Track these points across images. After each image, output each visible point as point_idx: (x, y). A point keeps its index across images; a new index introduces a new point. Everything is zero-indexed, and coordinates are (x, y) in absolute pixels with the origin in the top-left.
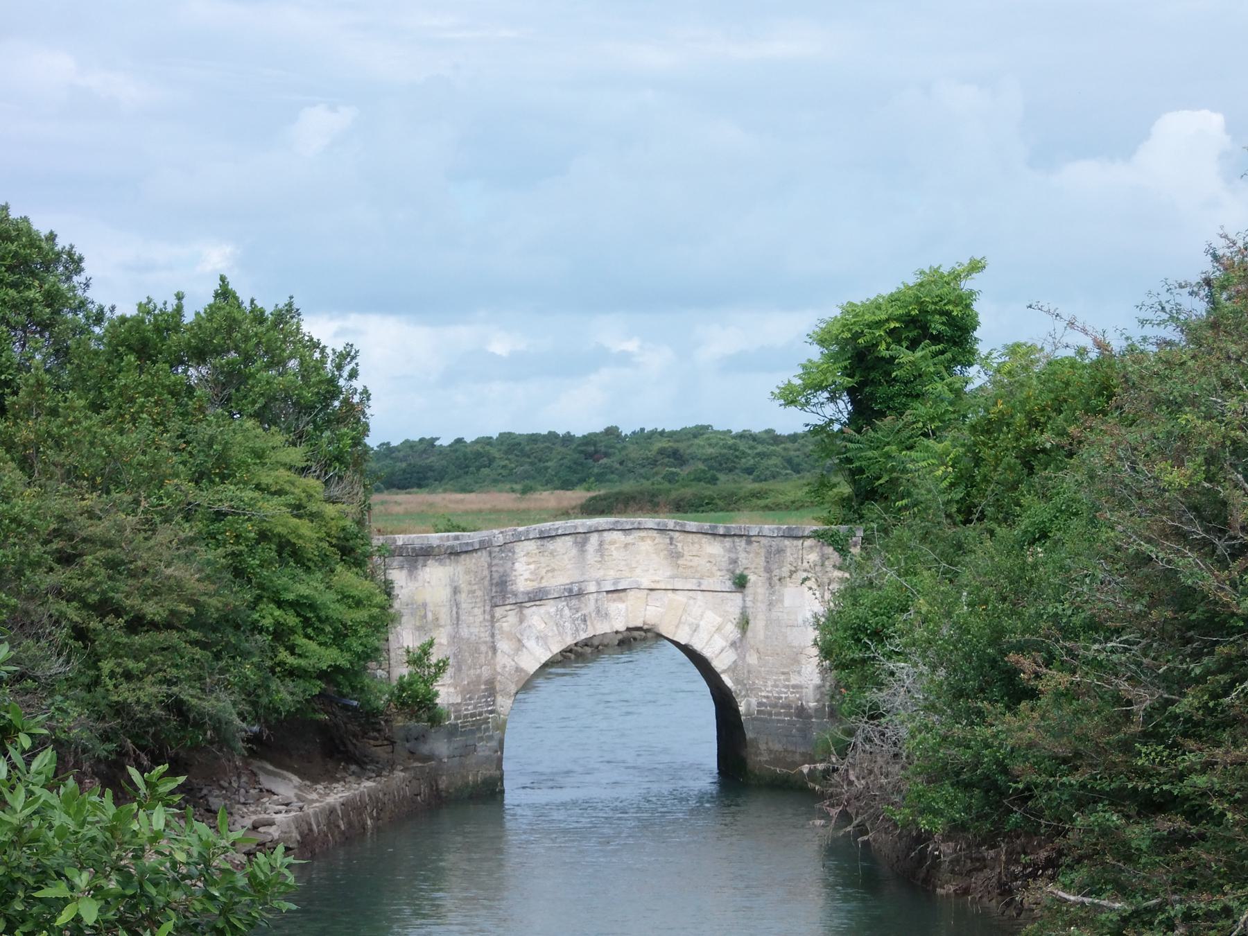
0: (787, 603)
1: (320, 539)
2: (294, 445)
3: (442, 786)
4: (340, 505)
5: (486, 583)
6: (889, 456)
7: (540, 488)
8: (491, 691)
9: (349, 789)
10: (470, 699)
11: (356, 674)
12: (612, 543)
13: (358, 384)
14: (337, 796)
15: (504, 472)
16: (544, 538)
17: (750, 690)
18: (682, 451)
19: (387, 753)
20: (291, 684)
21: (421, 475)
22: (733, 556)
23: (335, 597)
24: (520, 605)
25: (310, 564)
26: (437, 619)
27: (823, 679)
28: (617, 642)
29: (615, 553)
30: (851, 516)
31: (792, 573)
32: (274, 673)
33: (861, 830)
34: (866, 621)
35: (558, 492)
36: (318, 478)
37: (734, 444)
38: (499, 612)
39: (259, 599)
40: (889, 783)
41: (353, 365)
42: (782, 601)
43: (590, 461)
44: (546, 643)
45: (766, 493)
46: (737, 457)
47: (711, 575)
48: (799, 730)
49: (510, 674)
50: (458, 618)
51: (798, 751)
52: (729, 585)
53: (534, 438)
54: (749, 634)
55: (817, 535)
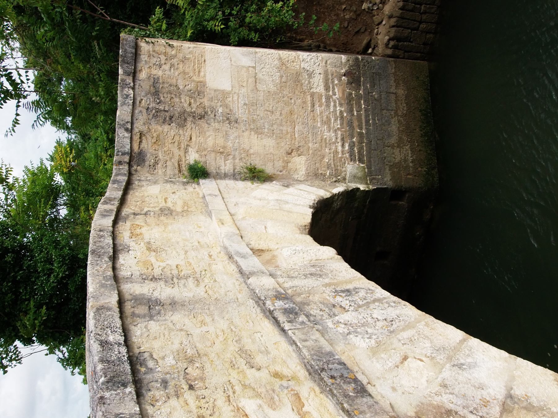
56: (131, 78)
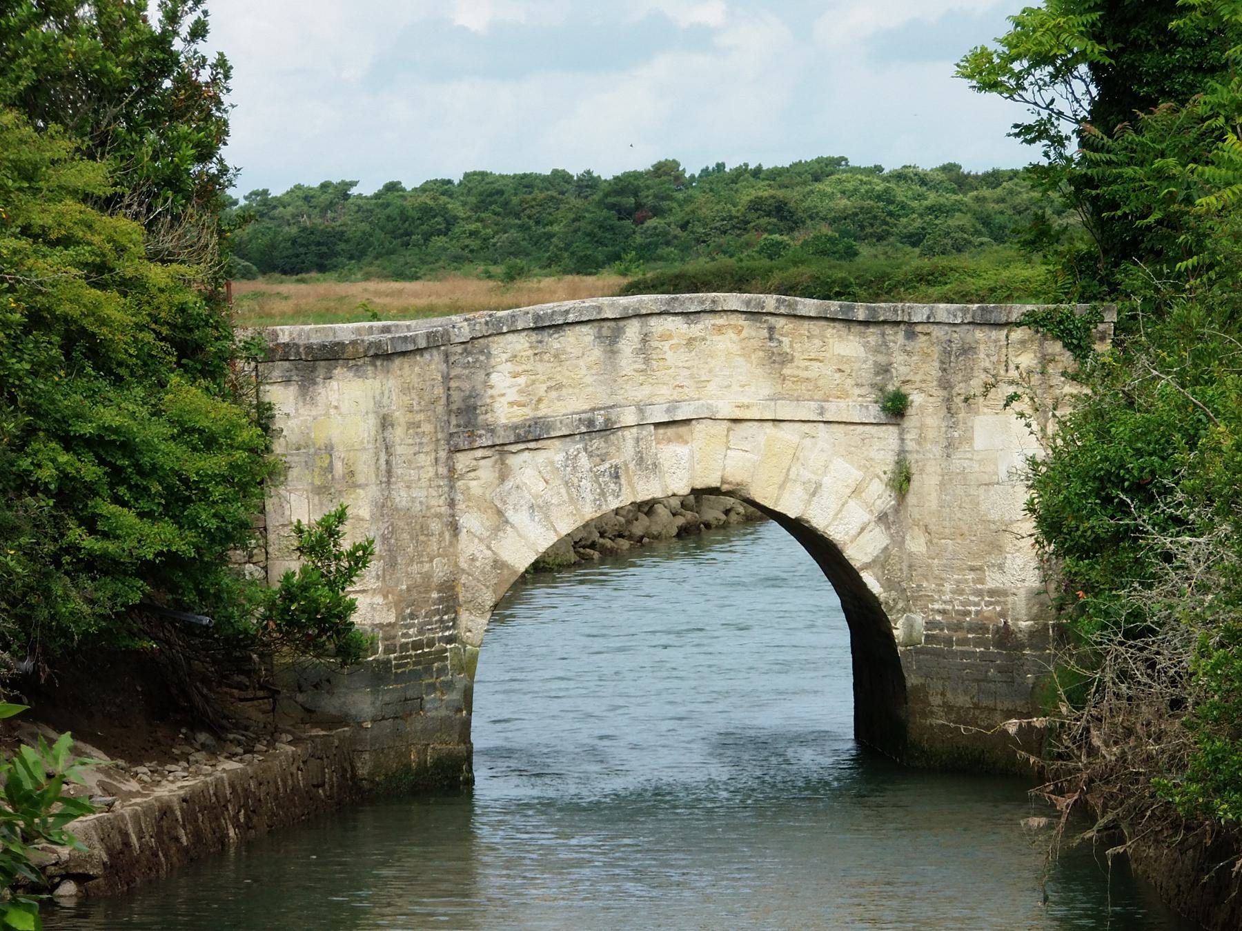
0: (979, 442)
1: (140, 327)
2: (92, 157)
3: (363, 771)
4: (175, 265)
5: (440, 409)
6: (1162, 176)
7: (537, 270)
8: (450, 601)
9: (197, 773)
10: (412, 616)
11: (208, 568)
12: (665, 337)
13: (207, 48)
14: (174, 787)
15: (474, 244)
16: (543, 328)
17: (913, 599)
18: (792, 204)
19: (264, 712)
20: (89, 585)
21: (324, 249)
22: (882, 359)
23: (168, 430)
24: (500, 448)
25: (122, 371)
26: (352, 473)
27: (1045, 580)
28: (674, 531)
29: (669, 355)
30: (1095, 288)
31: (988, 387)
32: (58, 565)
33: (1112, 835)
34: (1122, 466)
35: (569, 278)
36: (136, 217)
37: (886, 191)
38: (463, 461)
39: (30, 432)
40: (1163, 752)
41: (198, 14)
42: (970, 440)
43: (628, 223)
44: (547, 517)
45: (943, 274)
46: (891, 214)
47: (844, 395)
48: (1001, 670)
49: (482, 572)
50: (389, 472)
51: (999, 706)
52: (874, 412)
53: (526, 182)
54: (911, 499)
55: (1032, 321)
56: (971, 320)
